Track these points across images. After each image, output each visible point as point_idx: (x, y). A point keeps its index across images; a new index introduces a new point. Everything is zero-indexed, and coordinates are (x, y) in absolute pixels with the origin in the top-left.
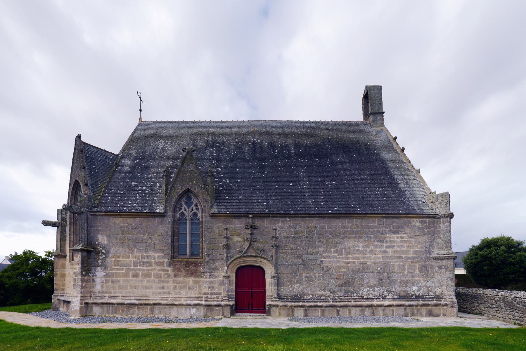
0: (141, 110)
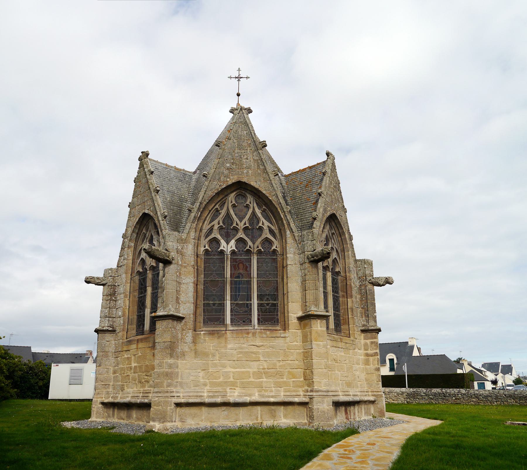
0: (238, 95)
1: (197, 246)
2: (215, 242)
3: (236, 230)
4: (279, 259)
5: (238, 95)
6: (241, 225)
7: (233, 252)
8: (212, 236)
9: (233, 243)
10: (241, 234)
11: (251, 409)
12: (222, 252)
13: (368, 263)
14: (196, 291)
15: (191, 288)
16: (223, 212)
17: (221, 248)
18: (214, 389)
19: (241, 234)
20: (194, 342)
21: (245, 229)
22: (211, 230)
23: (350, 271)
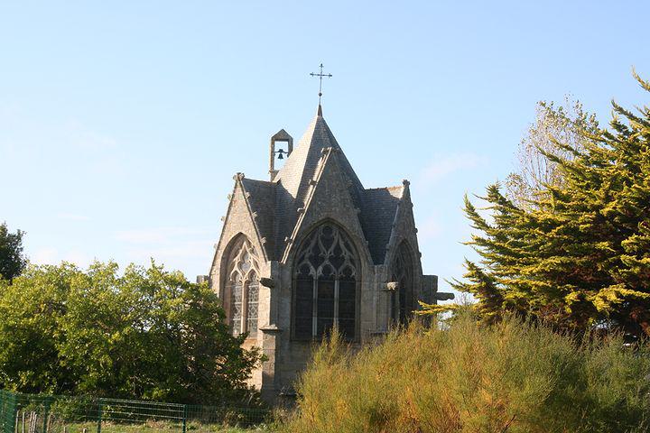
0: (320, 95)
1: (293, 272)
2: (306, 269)
3: (323, 259)
4: (357, 284)
5: (320, 95)
6: (328, 255)
7: (320, 278)
8: (304, 262)
9: (320, 268)
10: (327, 262)
11: (277, 279)
12: (311, 277)
13: (434, 279)
14: (292, 309)
15: (289, 306)
16: (313, 243)
17: (311, 273)
18: (171, 408)
19: (327, 262)
20: (290, 350)
21: (331, 259)
22: (303, 258)
23: (416, 288)
